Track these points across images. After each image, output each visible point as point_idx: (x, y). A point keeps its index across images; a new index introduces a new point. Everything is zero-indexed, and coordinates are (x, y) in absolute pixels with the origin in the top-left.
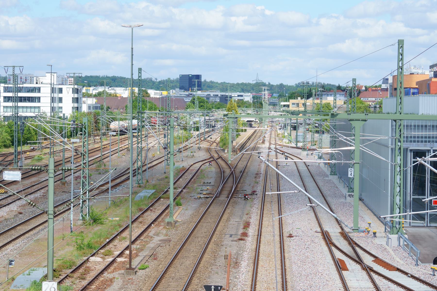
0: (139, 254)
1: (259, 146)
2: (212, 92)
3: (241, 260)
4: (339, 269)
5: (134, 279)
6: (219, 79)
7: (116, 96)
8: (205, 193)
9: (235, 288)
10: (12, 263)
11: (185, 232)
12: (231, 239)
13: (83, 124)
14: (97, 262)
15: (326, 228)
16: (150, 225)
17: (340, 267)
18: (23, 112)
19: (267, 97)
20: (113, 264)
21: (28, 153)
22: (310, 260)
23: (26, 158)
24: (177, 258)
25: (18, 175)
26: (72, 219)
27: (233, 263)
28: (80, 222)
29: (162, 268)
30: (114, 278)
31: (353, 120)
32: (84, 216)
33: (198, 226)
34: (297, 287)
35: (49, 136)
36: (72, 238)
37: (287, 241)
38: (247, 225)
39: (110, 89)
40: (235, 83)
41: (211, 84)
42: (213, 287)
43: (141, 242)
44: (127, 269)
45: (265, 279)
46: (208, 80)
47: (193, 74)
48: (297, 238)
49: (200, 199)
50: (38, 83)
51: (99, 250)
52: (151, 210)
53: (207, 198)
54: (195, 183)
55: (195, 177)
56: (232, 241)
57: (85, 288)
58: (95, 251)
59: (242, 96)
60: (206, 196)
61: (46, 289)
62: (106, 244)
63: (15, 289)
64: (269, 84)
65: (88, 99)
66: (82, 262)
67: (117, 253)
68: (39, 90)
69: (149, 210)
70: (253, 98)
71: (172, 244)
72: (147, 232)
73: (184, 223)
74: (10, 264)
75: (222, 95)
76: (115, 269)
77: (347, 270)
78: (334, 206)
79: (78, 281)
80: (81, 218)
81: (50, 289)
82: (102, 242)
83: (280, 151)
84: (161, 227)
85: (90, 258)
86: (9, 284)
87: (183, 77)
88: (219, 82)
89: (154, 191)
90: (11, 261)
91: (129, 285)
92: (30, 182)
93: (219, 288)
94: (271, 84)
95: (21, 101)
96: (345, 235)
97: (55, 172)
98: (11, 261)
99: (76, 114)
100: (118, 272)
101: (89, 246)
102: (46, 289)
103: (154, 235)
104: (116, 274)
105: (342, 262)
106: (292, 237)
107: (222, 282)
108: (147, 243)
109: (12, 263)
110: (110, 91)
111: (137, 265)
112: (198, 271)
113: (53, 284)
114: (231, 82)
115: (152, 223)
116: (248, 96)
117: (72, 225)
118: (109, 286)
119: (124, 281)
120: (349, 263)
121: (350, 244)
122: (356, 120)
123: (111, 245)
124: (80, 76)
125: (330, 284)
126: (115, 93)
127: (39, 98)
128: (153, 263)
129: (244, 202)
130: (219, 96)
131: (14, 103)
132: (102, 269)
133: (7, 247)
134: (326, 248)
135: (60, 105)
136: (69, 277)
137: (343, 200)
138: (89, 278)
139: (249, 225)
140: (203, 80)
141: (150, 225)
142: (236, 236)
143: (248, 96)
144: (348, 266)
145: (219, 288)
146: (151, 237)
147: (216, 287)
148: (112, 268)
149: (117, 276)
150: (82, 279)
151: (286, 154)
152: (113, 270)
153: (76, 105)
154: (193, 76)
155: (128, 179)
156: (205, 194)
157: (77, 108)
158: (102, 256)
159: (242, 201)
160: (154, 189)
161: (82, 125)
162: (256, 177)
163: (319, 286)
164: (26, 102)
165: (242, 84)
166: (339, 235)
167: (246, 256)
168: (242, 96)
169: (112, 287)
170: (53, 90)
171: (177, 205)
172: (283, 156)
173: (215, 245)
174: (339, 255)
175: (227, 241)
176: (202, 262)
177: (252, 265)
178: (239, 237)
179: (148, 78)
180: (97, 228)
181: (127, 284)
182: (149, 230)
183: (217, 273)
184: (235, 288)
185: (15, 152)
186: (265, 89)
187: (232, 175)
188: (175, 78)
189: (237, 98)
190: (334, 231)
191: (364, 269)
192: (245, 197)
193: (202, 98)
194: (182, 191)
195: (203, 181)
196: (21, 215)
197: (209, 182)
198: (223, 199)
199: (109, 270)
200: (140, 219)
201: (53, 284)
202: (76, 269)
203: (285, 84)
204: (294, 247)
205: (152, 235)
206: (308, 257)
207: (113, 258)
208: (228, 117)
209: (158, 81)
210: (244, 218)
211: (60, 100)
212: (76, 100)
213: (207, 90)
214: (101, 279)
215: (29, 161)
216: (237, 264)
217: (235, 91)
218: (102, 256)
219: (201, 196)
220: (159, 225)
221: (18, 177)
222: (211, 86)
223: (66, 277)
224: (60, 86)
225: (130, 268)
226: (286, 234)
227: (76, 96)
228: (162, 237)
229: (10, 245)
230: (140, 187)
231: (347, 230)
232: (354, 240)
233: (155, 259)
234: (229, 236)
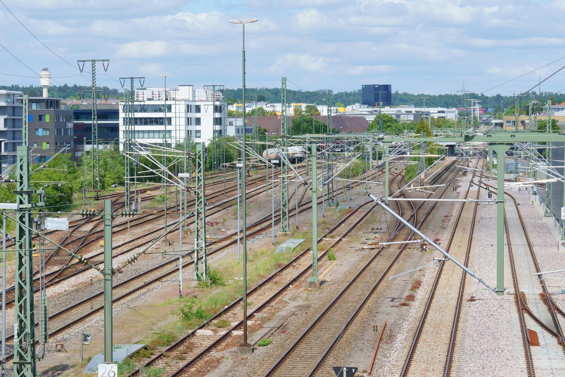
0: (265, 326)
1: (458, 178)
2: (404, 107)
3: (398, 333)
4: (527, 343)
5: (249, 358)
6: (415, 91)
7: (275, 115)
8: (370, 242)
9: (380, 371)
10: (88, 338)
11: (332, 295)
12: (392, 303)
13: (197, 153)
14: (206, 336)
15: (523, 288)
16: (288, 286)
17: (530, 339)
18: (154, 138)
19: (478, 113)
20: (226, 338)
21: (148, 192)
22: (491, 332)
23: (144, 200)
24: (314, 330)
25: (64, 223)
26: (181, 279)
27: (385, 336)
28: (195, 283)
29: (289, 344)
30: (223, 357)
31: (495, 144)
32: (200, 275)
33: (352, 287)
34: (466, 369)
35: (152, 170)
36: (180, 304)
37: (466, 306)
38: (417, 285)
39: (268, 105)
40: (437, 95)
41: (404, 97)
42: (345, 369)
43: (270, 309)
44: (241, 345)
45: (425, 357)
46: (401, 92)
47: (380, 84)
48: (481, 301)
49: (363, 251)
50: (169, 99)
51: (211, 321)
52: (294, 266)
53: (372, 249)
54: (360, 229)
55: (363, 221)
56: (392, 307)
57: (181, 371)
58: (205, 322)
59: (443, 112)
60: (370, 247)
61: (103, 374)
62: (221, 313)
63: (89, 373)
64: (483, 95)
65: (237, 119)
66: (185, 336)
67: (234, 324)
68: (169, 108)
69: (291, 267)
70: (460, 114)
71: (310, 312)
72: (282, 296)
73: (335, 283)
74: (85, 340)
75: (417, 112)
76: (227, 345)
77: (537, 344)
78: (540, 258)
79: (174, 361)
80: (196, 278)
81: (109, 374)
82: (218, 310)
83: (485, 185)
84: (302, 289)
85: (197, 331)
86: (83, 366)
87: (366, 88)
88: (416, 94)
89: (302, 240)
90: (86, 336)
91: (240, 367)
92: (143, 230)
93: (353, 370)
94: (485, 95)
95: (136, 123)
96: (546, 298)
97: (113, 218)
98: (86, 336)
99: (217, 139)
100: (230, 350)
101: (199, 315)
102: (103, 374)
103: (290, 299)
104: (226, 353)
105: (533, 334)
106: (474, 300)
107: (365, 362)
108: (278, 310)
109: (88, 338)
110: (268, 108)
111: (258, 341)
112: (337, 348)
113: (112, 367)
114: (432, 94)
115: (291, 283)
116: (452, 112)
117: (181, 288)
118: (215, 367)
119: (234, 362)
120: (544, 337)
121: (550, 309)
122: (499, 144)
123: (229, 314)
124: (222, 89)
125: (510, 365)
126: (274, 111)
127: (170, 119)
128: (279, 337)
129: (420, 253)
130: (413, 112)
131: (127, 127)
132: (209, 345)
133: (93, 317)
134: (516, 316)
135: (198, 128)
136: (164, 356)
137: (555, 250)
138: (190, 357)
139: (420, 285)
140: (393, 91)
141: (288, 286)
142: (399, 300)
143: (452, 112)
144: (541, 340)
145: (353, 370)
146: (286, 302)
147: (349, 370)
148: (224, 344)
149: (226, 355)
150: (181, 359)
151: (491, 189)
152: (225, 347)
153: (218, 128)
154: (380, 86)
155: (270, 226)
156: (371, 245)
157: (221, 131)
158: (213, 328)
159: (417, 253)
160: (303, 238)
161: (196, 154)
162: (444, 221)
163: (494, 366)
164: (152, 124)
165: (447, 96)
166: (539, 297)
167: (406, 326)
168: (443, 112)
169: (217, 371)
170: (189, 108)
171: (330, 259)
172: (487, 191)
173: (367, 312)
174: (531, 325)
175: (386, 306)
176: (344, 336)
177: (411, 339)
178: (403, 301)
179: (321, 91)
180: (216, 291)
181: (238, 366)
182: (285, 293)
183: (361, 350)
184: (380, 371)
185: (127, 191)
186: (474, 103)
187: (412, 218)
188: (357, 90)
189: (436, 116)
190: (531, 292)
191: (560, 344)
192: (422, 247)
193: (389, 116)
194: (340, 240)
195: (372, 226)
196: (120, 275)
197: (379, 227)
198: (393, 250)
199: (220, 347)
200: (277, 279)
201: (112, 367)
202: (175, 346)
203: (503, 95)
204: (474, 315)
205: (287, 300)
206: (489, 328)
207: (227, 331)
208: (383, 141)
209: (516, 95)
210: (415, 276)
211: (198, 121)
212: (218, 121)
213: (397, 105)
214: (206, 358)
215: (147, 203)
216: (391, 337)
217: (436, 106)
218: (213, 328)
219: (365, 247)
220: (299, 287)
221: (65, 226)
222: (405, 99)
223: (159, 357)
224: (197, 104)
225: (246, 344)
226: (466, 297)
227: (218, 115)
228: (300, 302)
229: (96, 314)
230: (286, 235)
231: (550, 290)
232: (557, 304)
233: (283, 332)
234: (390, 299)
